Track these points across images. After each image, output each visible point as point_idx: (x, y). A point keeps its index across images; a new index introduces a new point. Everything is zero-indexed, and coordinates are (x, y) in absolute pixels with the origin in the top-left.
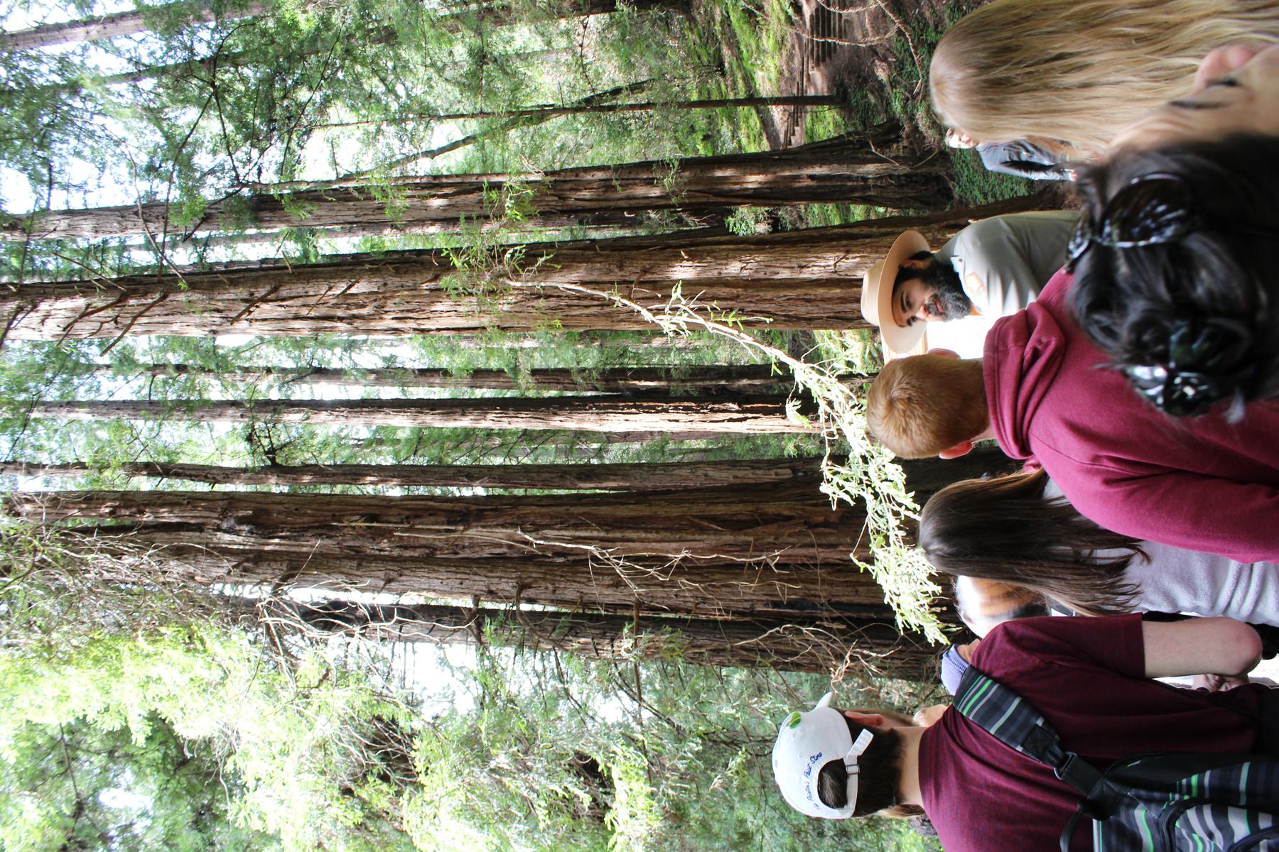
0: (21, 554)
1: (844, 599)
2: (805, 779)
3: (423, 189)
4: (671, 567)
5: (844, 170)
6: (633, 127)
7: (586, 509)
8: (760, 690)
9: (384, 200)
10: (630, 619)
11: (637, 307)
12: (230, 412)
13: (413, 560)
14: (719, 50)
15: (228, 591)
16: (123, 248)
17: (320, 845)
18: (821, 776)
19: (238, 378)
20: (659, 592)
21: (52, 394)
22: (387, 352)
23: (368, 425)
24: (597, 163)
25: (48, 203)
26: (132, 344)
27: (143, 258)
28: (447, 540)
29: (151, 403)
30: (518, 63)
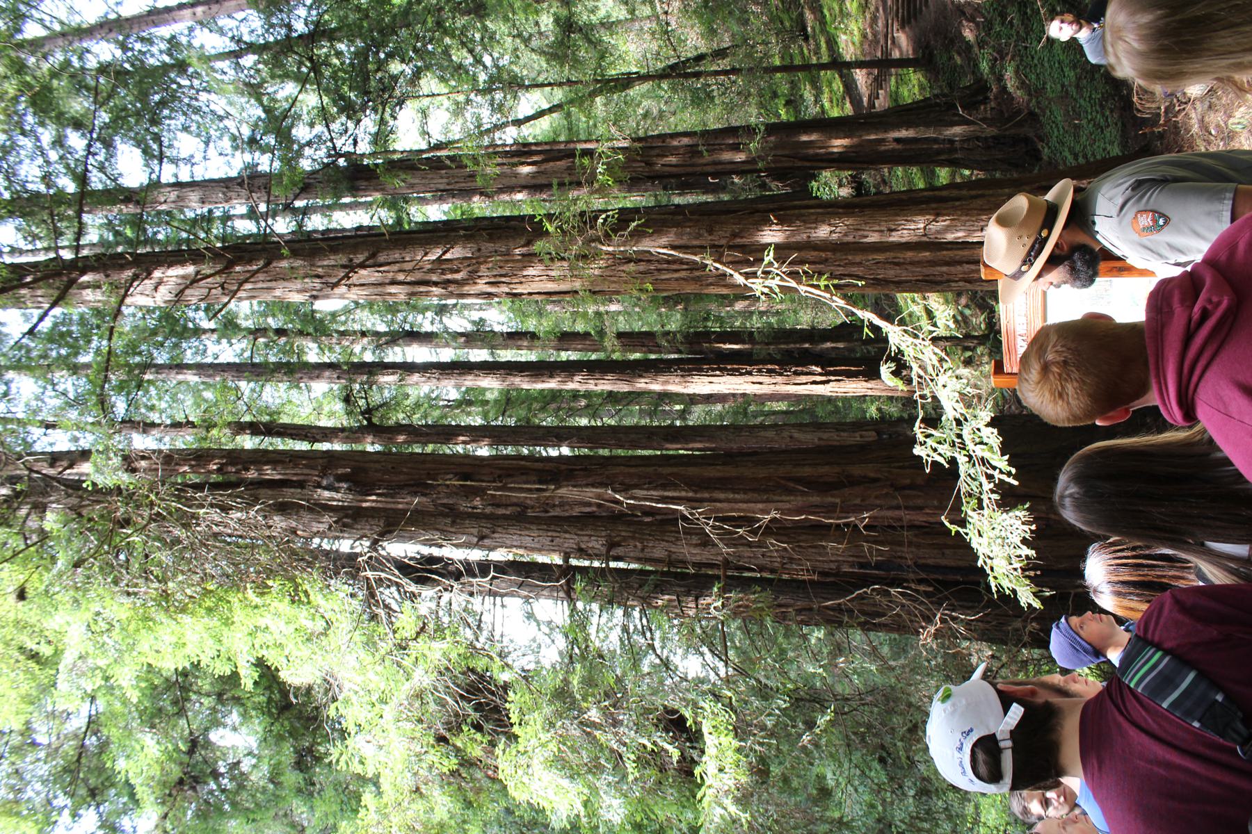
0: (138, 507)
1: (930, 562)
2: (957, 754)
3: (512, 156)
4: (760, 527)
5: (931, 133)
6: (715, 93)
7: (675, 470)
8: (838, 650)
9: (476, 168)
10: (718, 578)
11: (729, 271)
12: (327, 374)
13: (505, 517)
14: (802, 15)
15: (326, 545)
16: (227, 218)
17: (418, 789)
18: (973, 751)
19: (334, 341)
20: (746, 552)
21: (161, 358)
22: (476, 316)
23: (458, 387)
24: (680, 129)
25: (159, 177)
26: (234, 309)
27: (246, 227)
28: (537, 499)
29: (254, 365)
30: (602, 31)
